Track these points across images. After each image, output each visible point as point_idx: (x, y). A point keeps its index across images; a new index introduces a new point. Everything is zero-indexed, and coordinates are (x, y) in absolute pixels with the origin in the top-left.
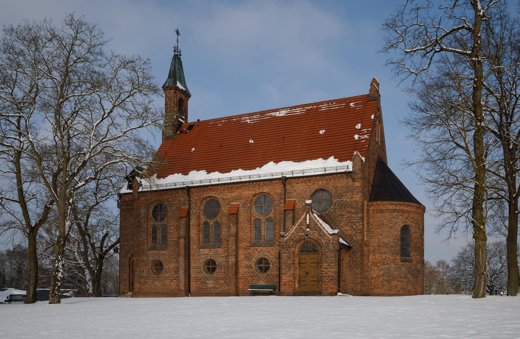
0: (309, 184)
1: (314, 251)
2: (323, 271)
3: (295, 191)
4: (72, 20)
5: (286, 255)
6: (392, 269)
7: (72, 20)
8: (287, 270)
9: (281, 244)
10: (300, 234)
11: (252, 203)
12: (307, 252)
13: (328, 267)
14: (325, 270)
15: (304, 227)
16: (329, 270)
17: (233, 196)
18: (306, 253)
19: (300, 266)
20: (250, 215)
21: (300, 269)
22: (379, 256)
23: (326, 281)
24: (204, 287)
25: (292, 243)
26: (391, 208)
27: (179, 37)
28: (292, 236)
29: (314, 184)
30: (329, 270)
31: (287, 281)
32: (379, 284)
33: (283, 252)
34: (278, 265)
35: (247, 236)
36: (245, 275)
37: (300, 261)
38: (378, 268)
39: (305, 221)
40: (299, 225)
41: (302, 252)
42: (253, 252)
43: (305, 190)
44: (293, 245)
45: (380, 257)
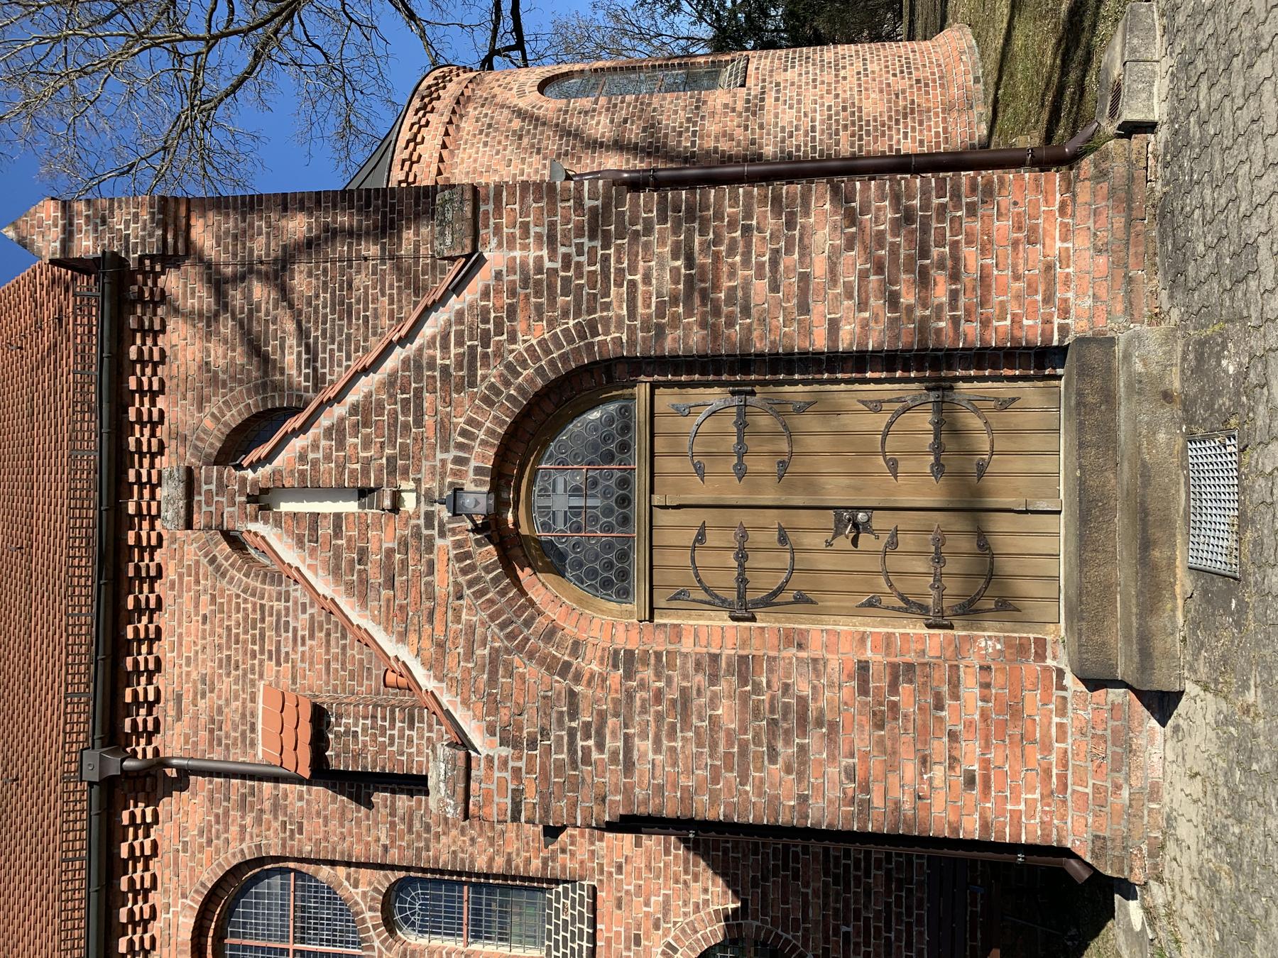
0: (173, 576)
1: (625, 447)
3: (207, 684)
5: (644, 746)
9: (531, 798)
10: (443, 581)
12: (625, 521)
14: (819, 311)
15: (383, 538)
16: (819, 267)
18: (637, 531)
19: (768, 602)
21: (801, 599)
28: (455, 664)
33: (612, 776)
34: (257, 21)
37: (715, 601)
39: (325, 530)
40: (361, 591)
41: (624, 575)
43: (205, 609)
44: (550, 665)
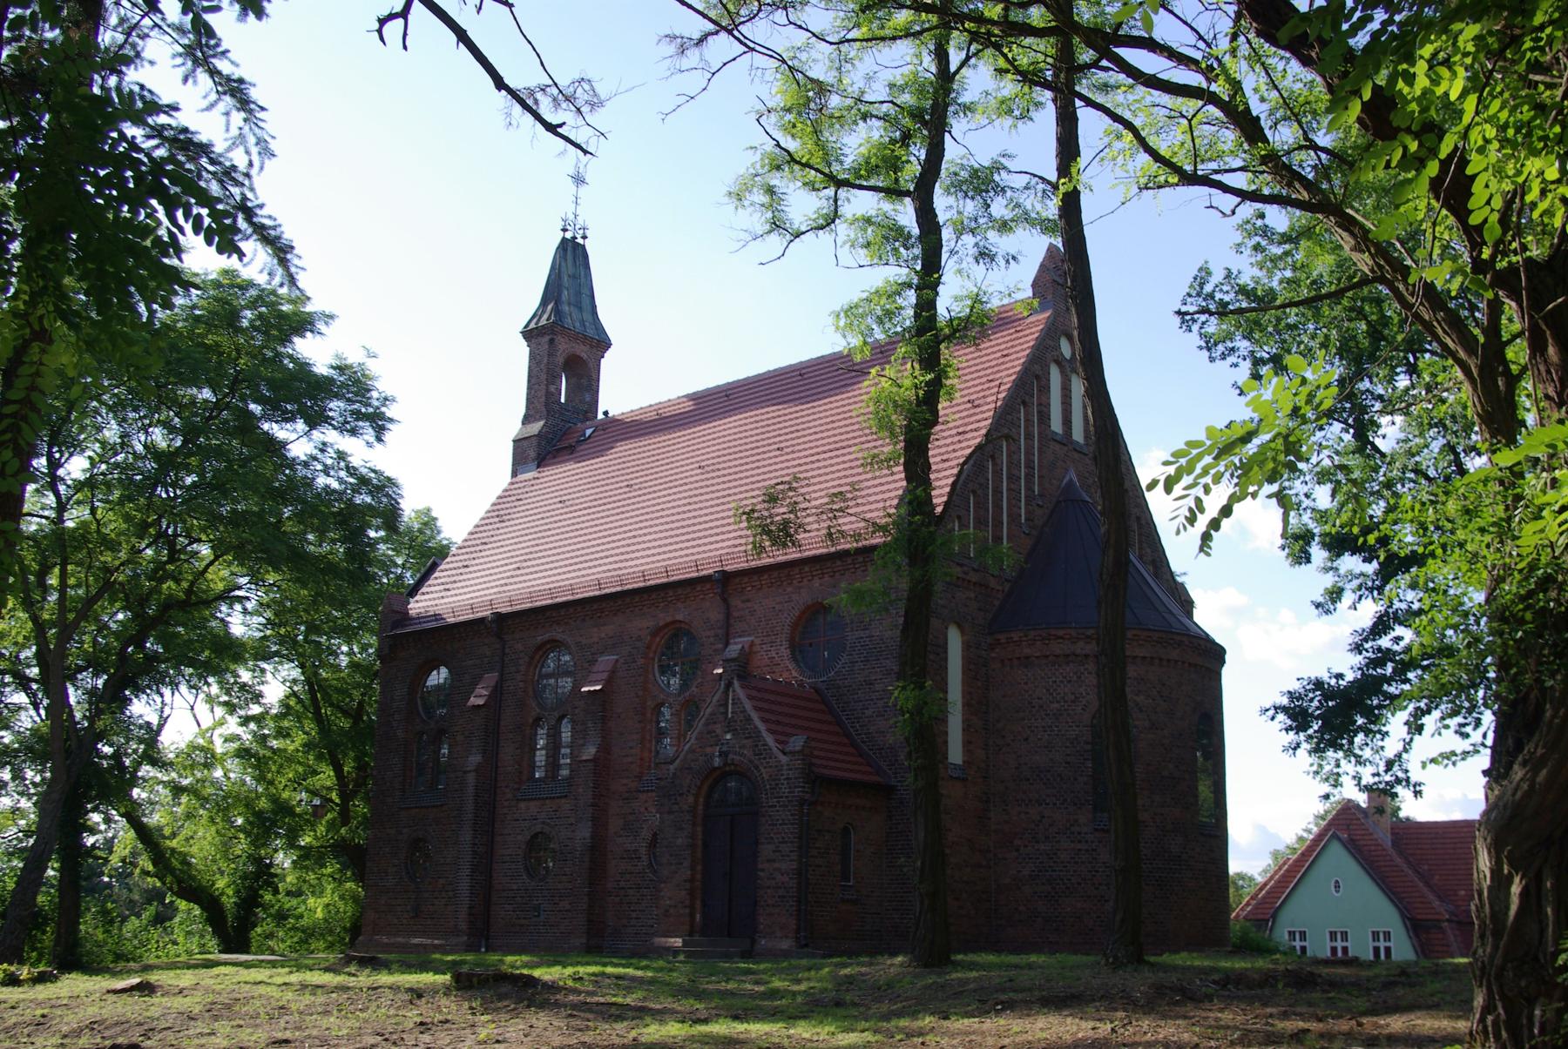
4: (1318, 606)
7: (1318, 606)
11: (651, 655)
16: (777, 865)
17: (603, 635)
20: (640, 693)
23: (770, 902)
24: (523, 922)
26: (1058, 652)
27: (583, 190)
29: (800, 588)
30: (777, 865)
35: (630, 759)
36: (622, 884)
42: (642, 810)
43: (777, 607)
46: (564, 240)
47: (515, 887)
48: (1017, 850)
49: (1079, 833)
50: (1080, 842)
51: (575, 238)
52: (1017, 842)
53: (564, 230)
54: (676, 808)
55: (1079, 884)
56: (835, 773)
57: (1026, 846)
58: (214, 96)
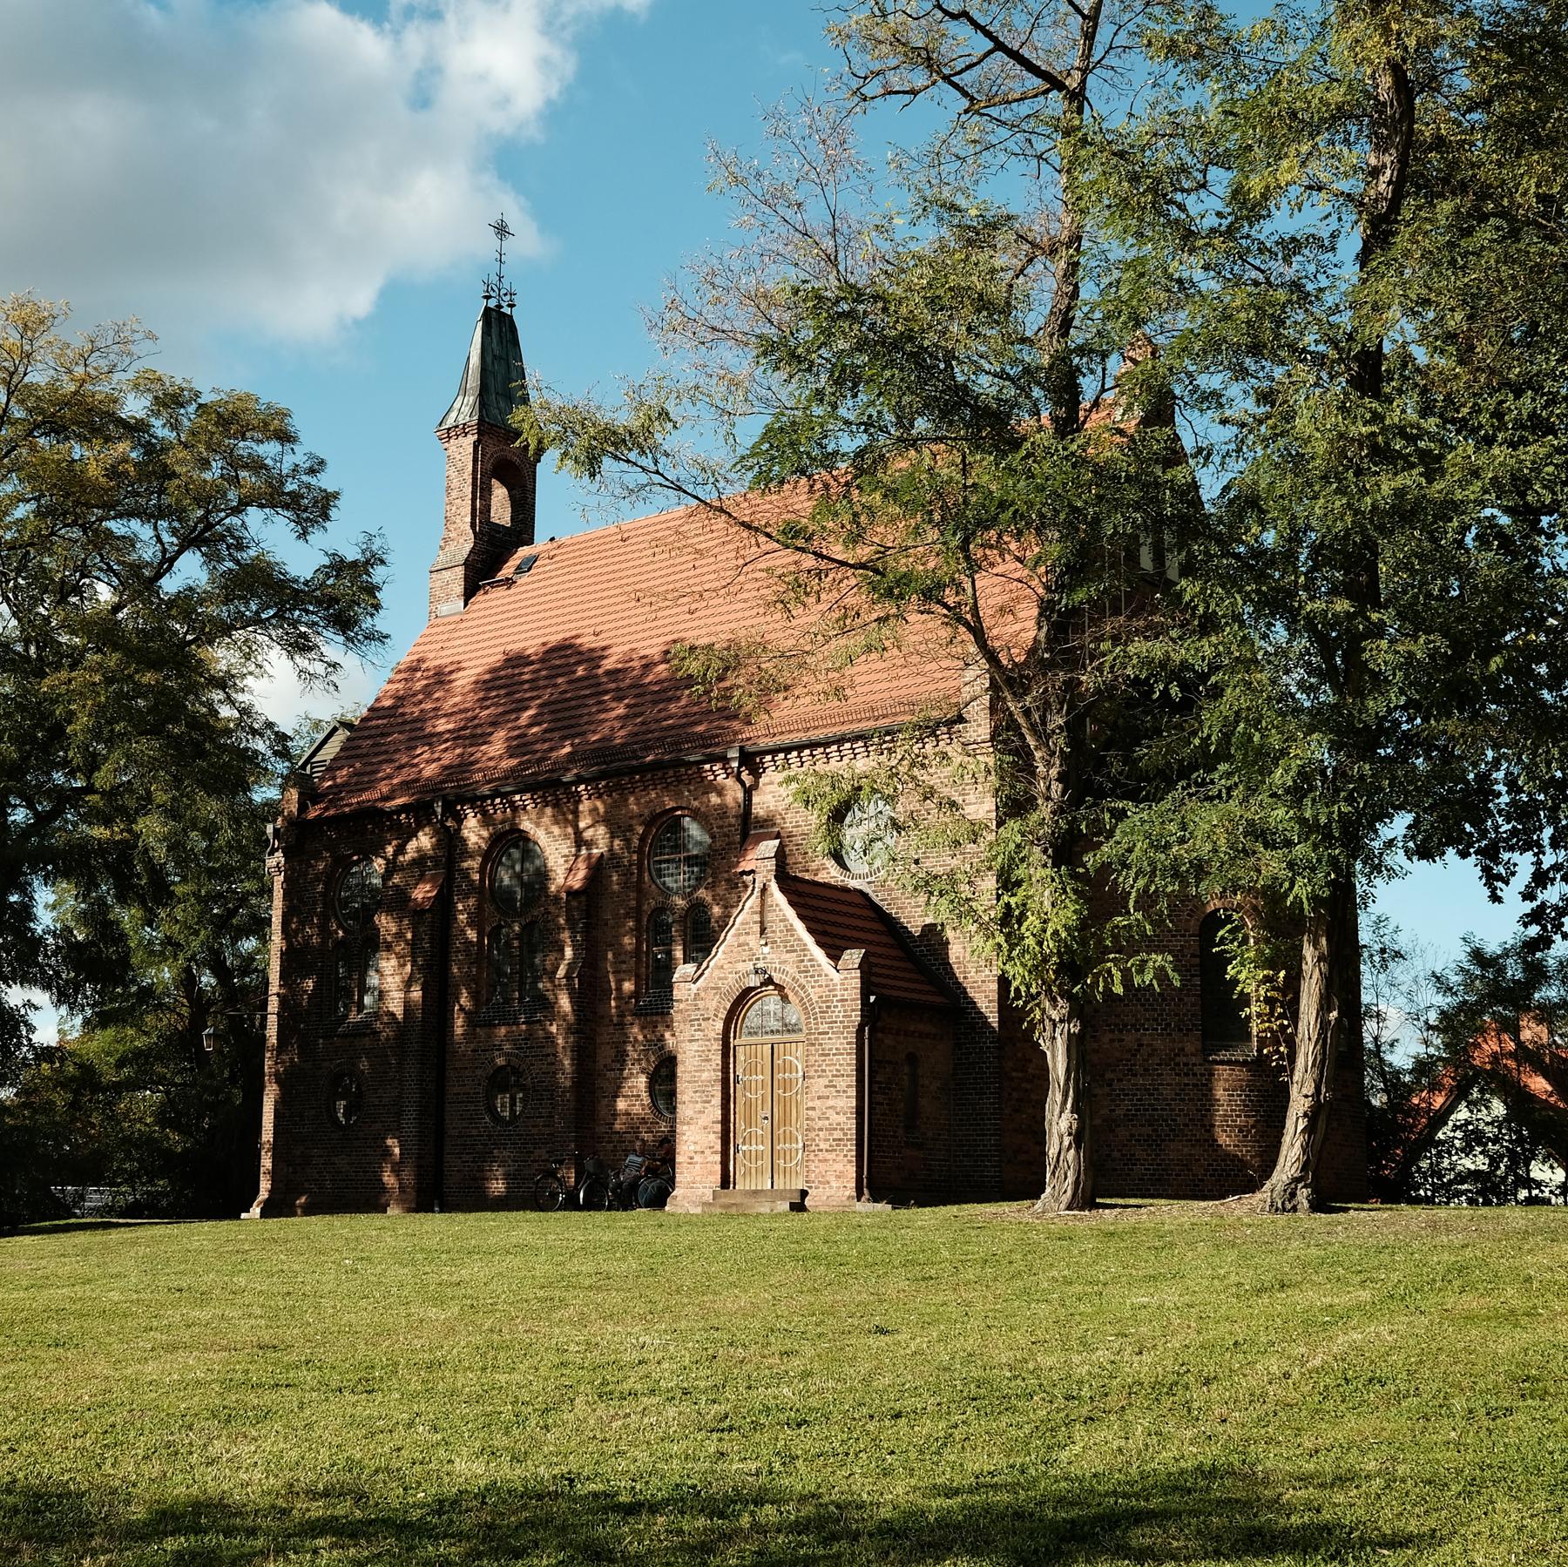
2: (813, 1109)
5: (695, 1046)
6: (1167, 1092)
8: (699, 1106)
13: (826, 1092)
14: (817, 1103)
16: (830, 1103)
22: (1112, 1041)
23: (822, 1146)
25: (714, 1003)
27: (509, 243)
30: (830, 1103)
31: (698, 1148)
32: (1116, 1154)
38: (1107, 1089)
45: (1116, 1044)
46: (487, 310)
47: (474, 1132)
48: (1110, 1085)
49: (1186, 1064)
50: (1187, 1075)
51: (500, 306)
52: (1109, 1075)
53: (488, 298)
54: (698, 1035)
55: (1186, 1125)
56: (895, 993)
57: (1120, 1080)
58: (743, 319)
